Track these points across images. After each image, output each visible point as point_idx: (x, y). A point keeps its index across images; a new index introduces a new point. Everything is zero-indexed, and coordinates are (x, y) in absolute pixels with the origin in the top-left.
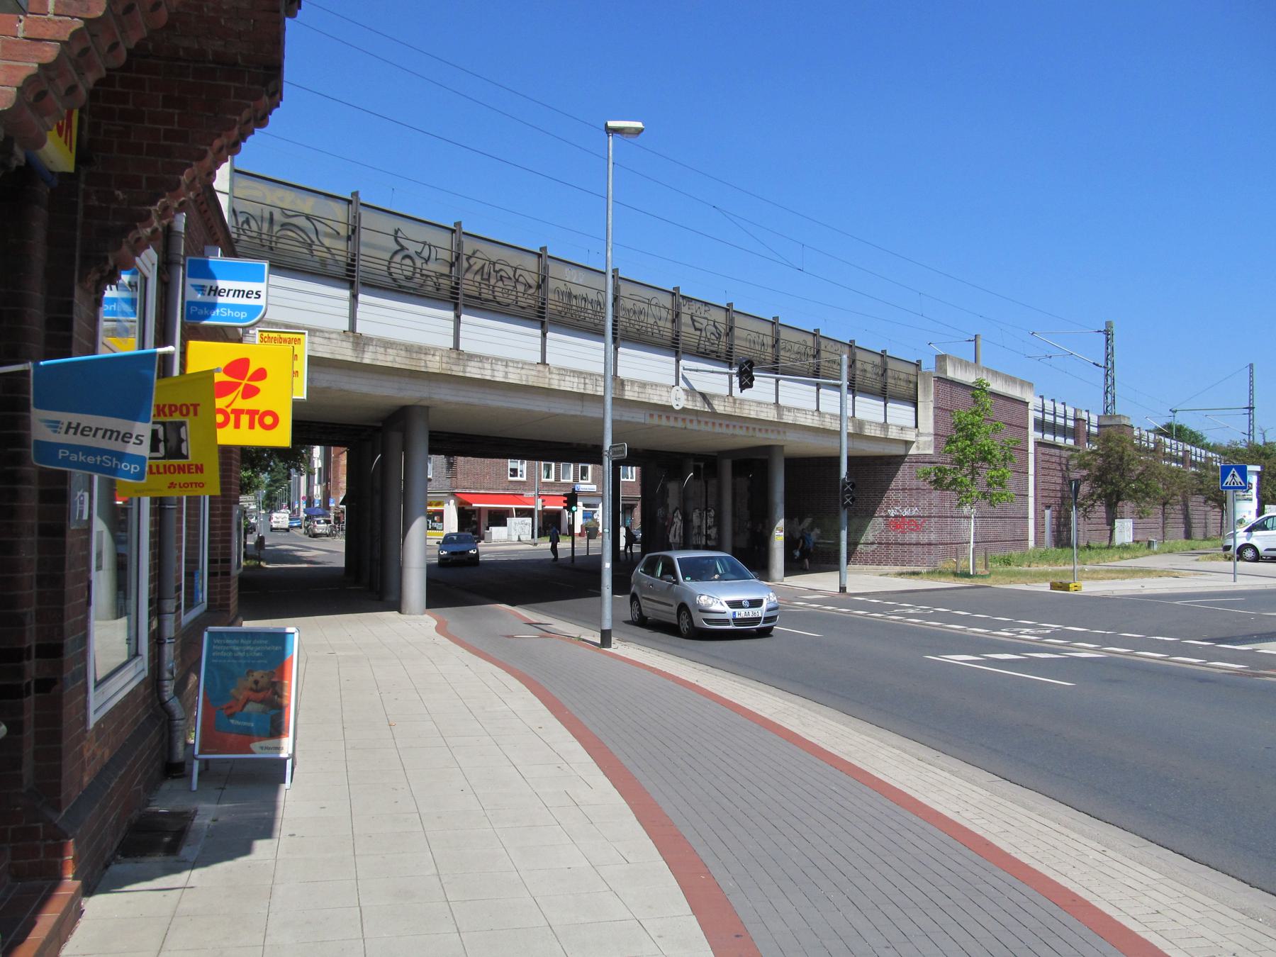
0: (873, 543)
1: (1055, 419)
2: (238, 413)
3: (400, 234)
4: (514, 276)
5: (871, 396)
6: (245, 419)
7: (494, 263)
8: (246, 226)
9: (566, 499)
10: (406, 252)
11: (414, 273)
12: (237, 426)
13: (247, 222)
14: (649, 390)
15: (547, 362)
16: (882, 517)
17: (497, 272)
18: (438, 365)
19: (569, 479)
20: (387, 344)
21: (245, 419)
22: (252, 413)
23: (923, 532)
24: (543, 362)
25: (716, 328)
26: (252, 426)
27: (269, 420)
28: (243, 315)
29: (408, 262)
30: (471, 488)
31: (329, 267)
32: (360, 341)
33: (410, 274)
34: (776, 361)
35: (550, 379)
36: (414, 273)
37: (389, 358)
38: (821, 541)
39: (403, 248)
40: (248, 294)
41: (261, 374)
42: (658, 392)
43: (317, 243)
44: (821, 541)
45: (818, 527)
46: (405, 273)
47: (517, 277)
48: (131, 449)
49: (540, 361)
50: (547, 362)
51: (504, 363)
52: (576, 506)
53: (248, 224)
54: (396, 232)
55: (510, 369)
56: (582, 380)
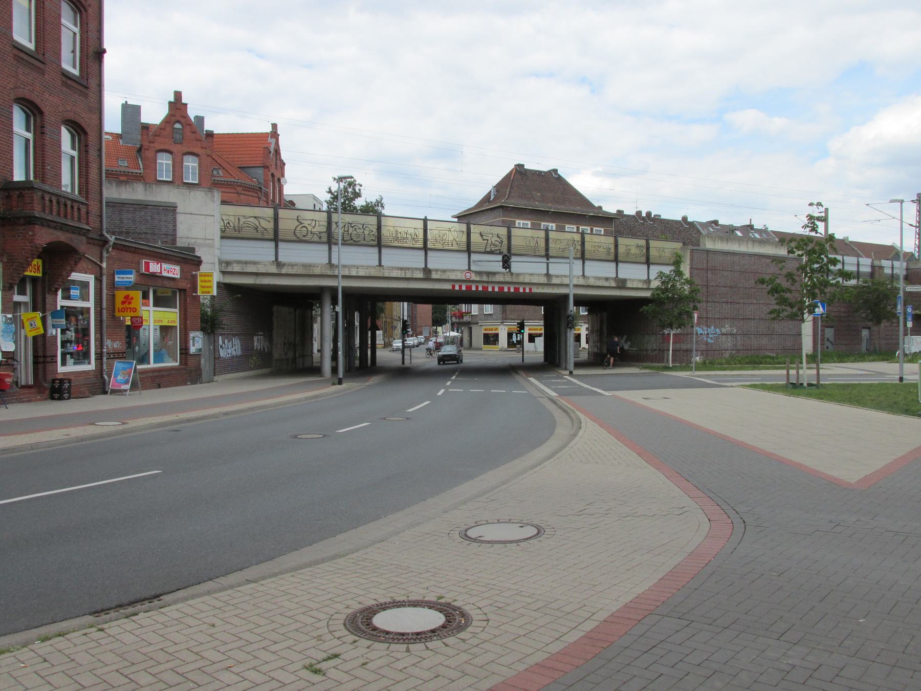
0: (656, 350)
1: (858, 268)
2: (127, 308)
3: (299, 218)
4: (363, 228)
5: (762, 254)
6: (129, 310)
7: (351, 224)
8: (228, 225)
9: (519, 326)
10: (303, 225)
11: (307, 234)
12: (127, 311)
13: (229, 223)
14: (448, 273)
15: (382, 265)
16: (661, 334)
17: (353, 227)
18: (319, 271)
19: (582, 312)
20: (292, 265)
21: (129, 310)
22: (130, 308)
23: (684, 343)
24: (380, 265)
25: (499, 237)
26: (130, 312)
27: (134, 310)
28: (128, 283)
29: (305, 229)
30: (516, 319)
31: (265, 236)
32: (279, 264)
33: (305, 234)
34: (547, 249)
35: (383, 272)
36: (307, 234)
37: (294, 270)
38: (631, 349)
39: (301, 223)
40: (129, 278)
41: (132, 298)
42: (455, 274)
43: (260, 227)
44: (631, 349)
45: (629, 341)
46: (304, 234)
47: (364, 228)
48: (63, 323)
49: (378, 265)
50: (382, 265)
51: (356, 267)
52: (524, 330)
53: (229, 224)
54: (298, 217)
55: (360, 270)
56: (404, 272)
